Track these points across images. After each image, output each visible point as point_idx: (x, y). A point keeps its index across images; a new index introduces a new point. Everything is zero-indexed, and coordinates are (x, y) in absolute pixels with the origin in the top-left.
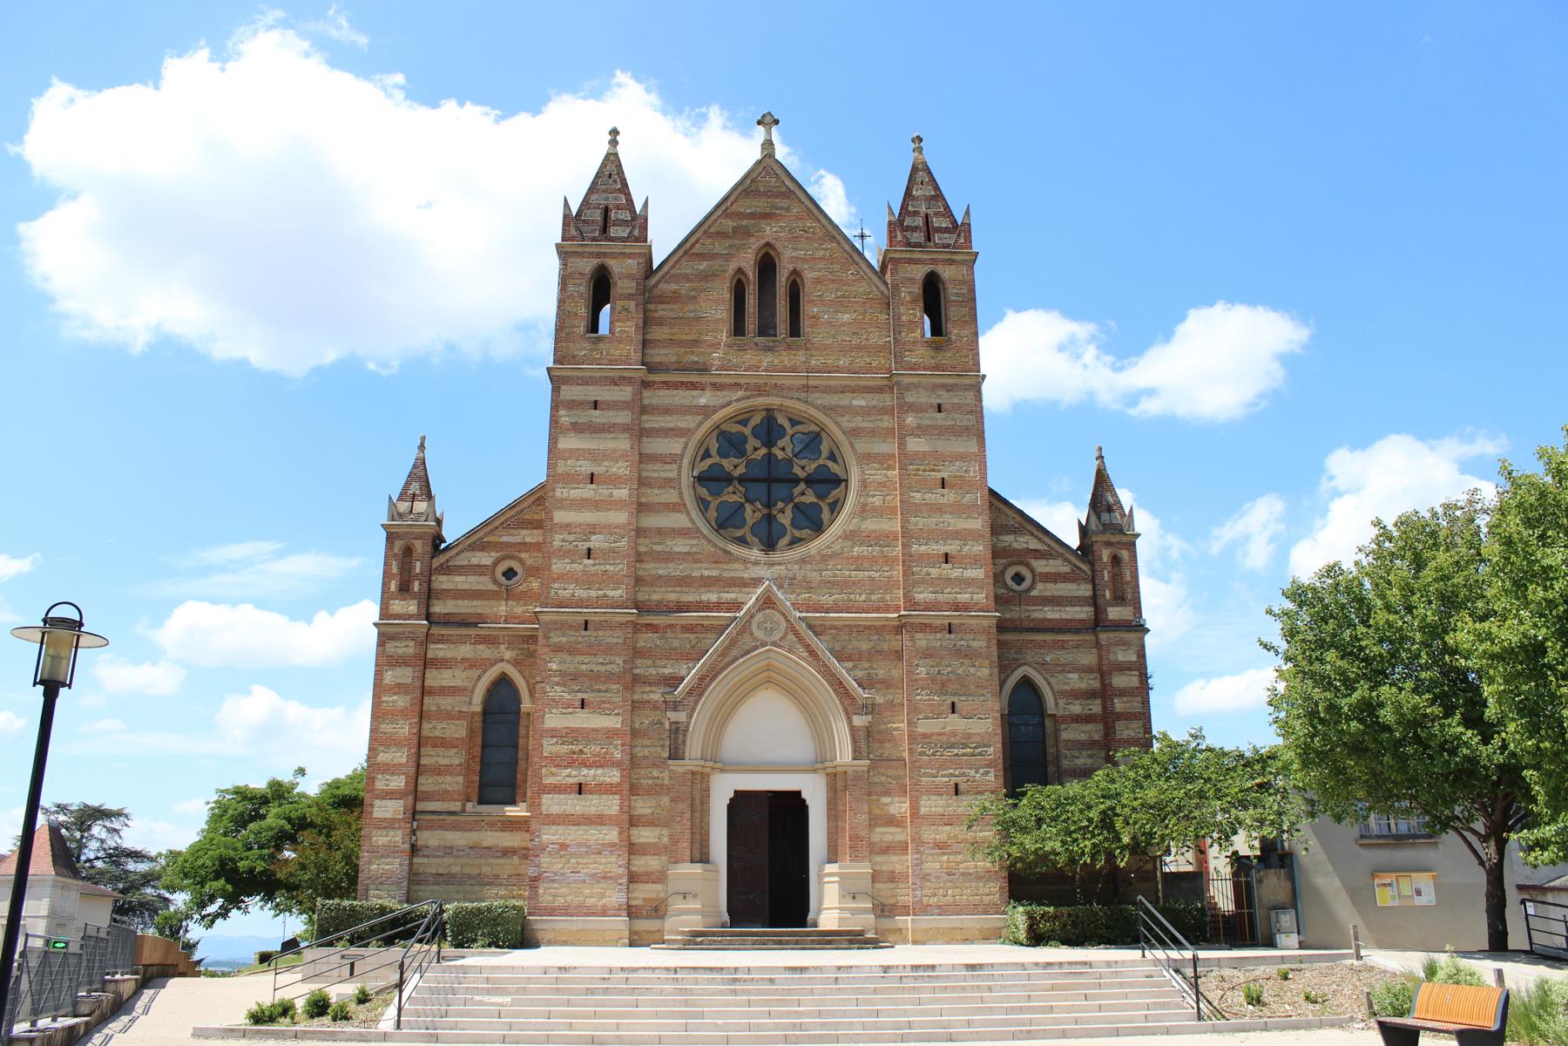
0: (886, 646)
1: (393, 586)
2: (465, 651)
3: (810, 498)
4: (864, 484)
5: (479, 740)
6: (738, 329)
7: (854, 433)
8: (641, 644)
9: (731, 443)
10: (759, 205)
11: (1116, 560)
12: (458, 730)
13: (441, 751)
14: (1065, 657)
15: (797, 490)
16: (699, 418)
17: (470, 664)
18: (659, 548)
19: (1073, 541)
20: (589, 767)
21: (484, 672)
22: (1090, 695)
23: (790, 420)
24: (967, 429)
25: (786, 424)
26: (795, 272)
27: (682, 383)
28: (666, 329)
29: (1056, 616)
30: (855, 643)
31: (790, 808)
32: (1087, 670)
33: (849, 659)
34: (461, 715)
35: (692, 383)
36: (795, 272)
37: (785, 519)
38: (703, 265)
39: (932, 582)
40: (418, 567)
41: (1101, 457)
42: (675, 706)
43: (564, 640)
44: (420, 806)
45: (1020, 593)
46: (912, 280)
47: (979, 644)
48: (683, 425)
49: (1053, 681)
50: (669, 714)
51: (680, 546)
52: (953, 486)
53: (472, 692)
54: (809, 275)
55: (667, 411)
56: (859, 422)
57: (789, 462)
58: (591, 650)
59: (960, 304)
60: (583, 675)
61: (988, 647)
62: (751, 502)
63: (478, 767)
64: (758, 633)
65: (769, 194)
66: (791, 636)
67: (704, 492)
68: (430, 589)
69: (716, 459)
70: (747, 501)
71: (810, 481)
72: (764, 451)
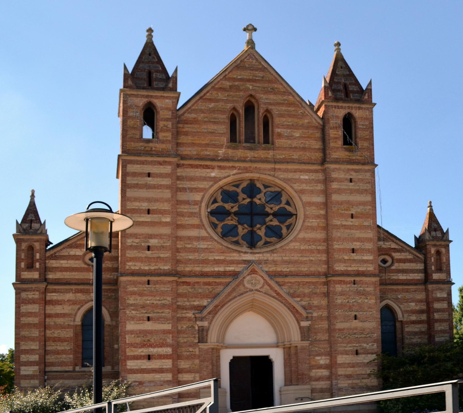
0: (318, 291)
1: (23, 265)
2: (70, 296)
3: (275, 223)
4: (306, 217)
5: (80, 338)
6: (233, 138)
7: (301, 192)
8: (180, 291)
9: (229, 195)
10: (246, 74)
11: (438, 253)
12: (69, 333)
13: (58, 344)
14: (408, 296)
15: (268, 219)
16: (211, 183)
17: (74, 303)
18: (189, 246)
19: (413, 245)
20: (155, 347)
21: (82, 306)
22: (421, 312)
23: (264, 185)
24: (366, 190)
25: (262, 187)
26: (267, 111)
27: (201, 165)
28: (190, 138)
29: (404, 278)
30: (301, 289)
31: (264, 364)
32: (421, 301)
33: (298, 296)
34: (69, 326)
35: (206, 166)
36: (267, 111)
37: (262, 232)
38: (212, 105)
39: (345, 261)
40: (38, 256)
41: (431, 206)
42: (202, 319)
43: (136, 289)
44: (48, 369)
45: (385, 268)
46: (337, 117)
47: (370, 289)
48: (201, 186)
49: (402, 306)
50: (198, 323)
51: (203, 245)
52: (357, 217)
53: (75, 315)
54: (275, 110)
55: (192, 179)
56: (304, 186)
57: (263, 206)
58: (152, 294)
59: (364, 130)
60: (148, 305)
61: (375, 290)
62: (242, 224)
63: (81, 351)
64: (247, 285)
65: (252, 68)
66: (266, 287)
67: (214, 220)
68: (45, 267)
69: (220, 204)
70: (240, 224)
71: (275, 215)
72: (248, 200)
